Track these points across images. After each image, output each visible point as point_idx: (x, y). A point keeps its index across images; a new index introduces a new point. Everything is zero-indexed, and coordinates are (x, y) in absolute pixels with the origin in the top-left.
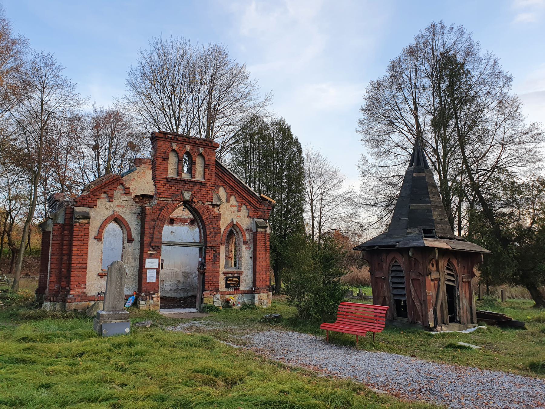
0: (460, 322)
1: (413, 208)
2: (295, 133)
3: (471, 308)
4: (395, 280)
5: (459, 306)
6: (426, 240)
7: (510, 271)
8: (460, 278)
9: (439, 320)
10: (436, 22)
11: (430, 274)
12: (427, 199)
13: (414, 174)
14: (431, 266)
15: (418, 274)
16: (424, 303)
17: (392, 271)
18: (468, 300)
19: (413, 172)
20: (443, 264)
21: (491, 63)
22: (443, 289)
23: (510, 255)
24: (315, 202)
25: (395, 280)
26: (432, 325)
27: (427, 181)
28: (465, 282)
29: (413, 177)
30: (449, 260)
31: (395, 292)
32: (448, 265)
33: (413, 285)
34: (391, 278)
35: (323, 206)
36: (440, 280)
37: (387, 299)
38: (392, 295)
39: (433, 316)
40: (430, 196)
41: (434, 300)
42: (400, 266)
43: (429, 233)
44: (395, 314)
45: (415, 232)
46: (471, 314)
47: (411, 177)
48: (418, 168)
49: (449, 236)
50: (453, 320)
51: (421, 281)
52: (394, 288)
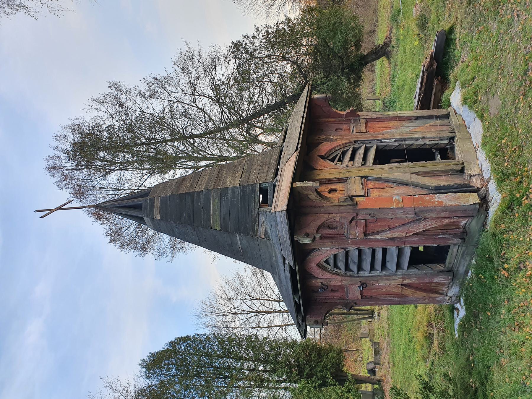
0: (452, 138)
1: (218, 223)
2: (160, 346)
3: (418, 118)
4: (367, 265)
5: (418, 139)
6: (276, 205)
7: (345, 87)
8: (360, 138)
9: (457, 180)
10: (45, 164)
11: (352, 198)
12: (202, 196)
13: (157, 216)
14: (333, 196)
15: (353, 223)
16: (419, 215)
17: (347, 268)
18: (404, 123)
19: (153, 220)
20: (328, 170)
21: (98, 105)
22: (387, 170)
23: (323, 81)
24: (262, 308)
25: (367, 265)
26: (473, 199)
27: (169, 193)
28: (367, 127)
29: (162, 219)
30: (323, 157)
31: (392, 265)
32: (333, 160)
33: (378, 233)
34: (361, 273)
35: (266, 298)
36: (366, 177)
37: (407, 282)
38: (400, 272)
39: (453, 195)
40: (197, 189)
41: (411, 190)
42: (335, 256)
43: (267, 195)
44: (440, 267)
45: (264, 225)
46: (430, 117)
47: (162, 223)
48: (146, 209)
49: (276, 157)
50: (446, 152)
51: (368, 217)
52: (384, 266)
